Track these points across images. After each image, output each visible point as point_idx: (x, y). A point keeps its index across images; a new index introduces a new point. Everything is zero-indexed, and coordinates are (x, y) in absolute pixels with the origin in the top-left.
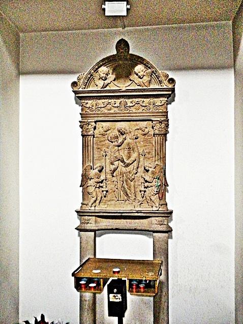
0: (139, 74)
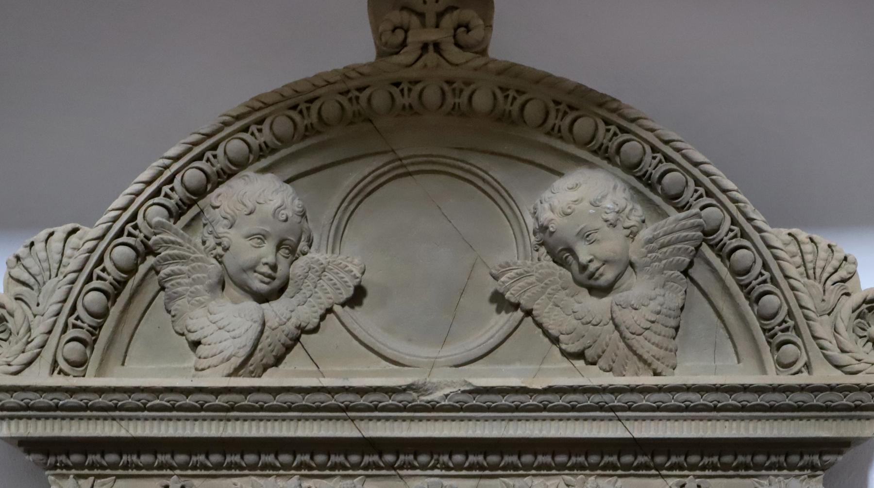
0: (584, 253)
